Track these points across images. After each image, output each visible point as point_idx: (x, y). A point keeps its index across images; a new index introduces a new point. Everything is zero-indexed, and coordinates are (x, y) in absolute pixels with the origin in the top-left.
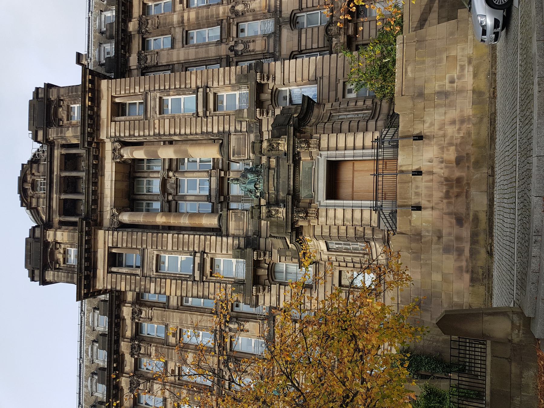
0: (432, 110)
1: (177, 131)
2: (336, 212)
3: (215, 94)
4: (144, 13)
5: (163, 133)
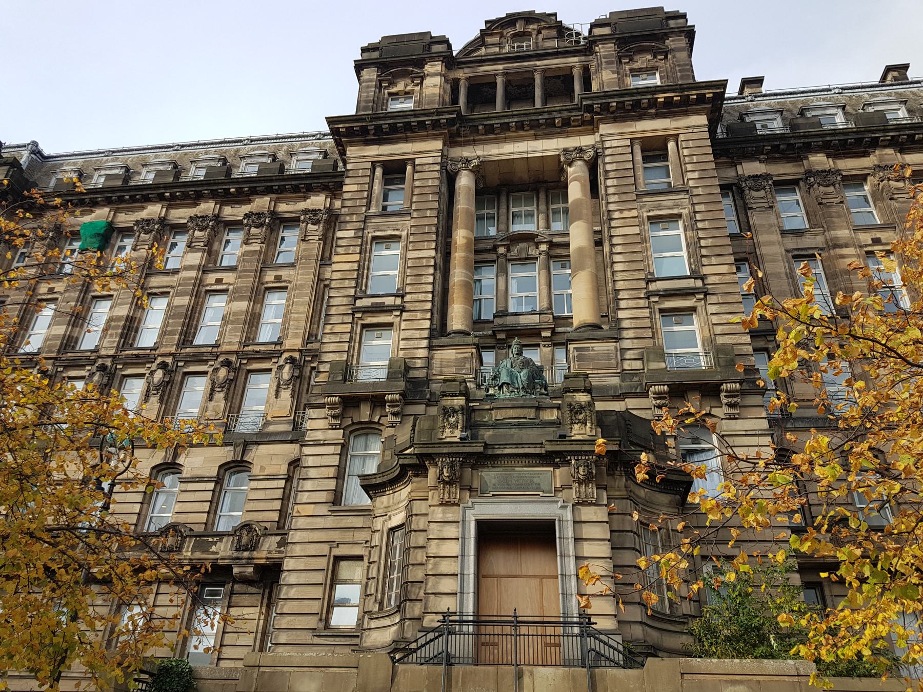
1: (618, 249)
2: (453, 542)
3: (694, 309)
4: (845, 178)
5: (613, 225)
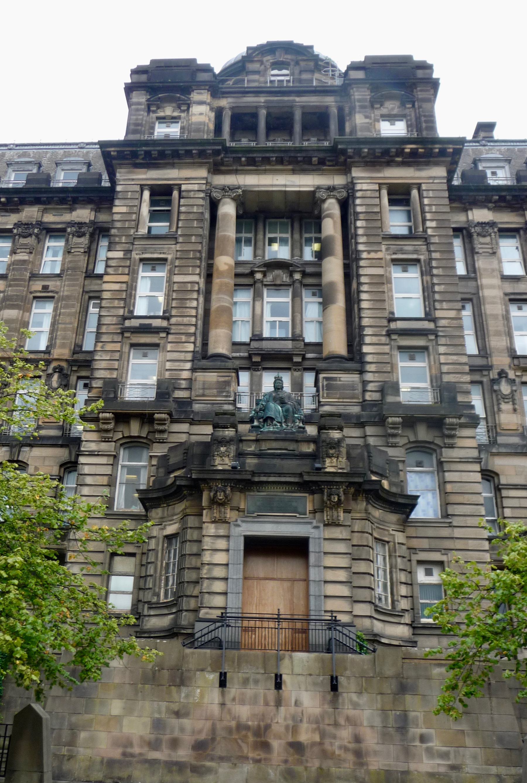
0: (379, 706)
